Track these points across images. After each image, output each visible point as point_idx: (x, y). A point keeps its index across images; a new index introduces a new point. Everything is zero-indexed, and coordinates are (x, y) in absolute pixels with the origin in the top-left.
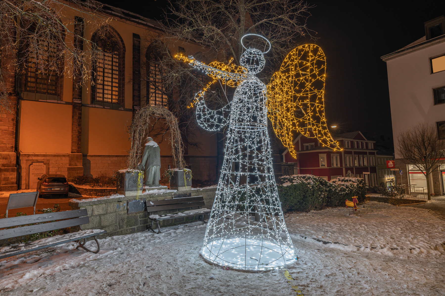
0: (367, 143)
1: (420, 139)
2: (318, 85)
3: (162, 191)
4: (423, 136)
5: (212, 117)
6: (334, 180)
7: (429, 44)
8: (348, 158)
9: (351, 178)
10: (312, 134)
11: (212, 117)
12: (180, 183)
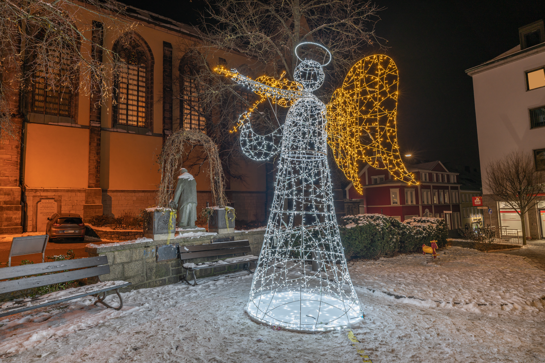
0: (448, 176)
1: (513, 171)
2: (389, 104)
3: (199, 234)
4: (517, 167)
5: (260, 144)
6: (409, 220)
7: (524, 54)
8: (425, 193)
9: (429, 219)
10: (381, 165)
11: (260, 144)
12: (220, 224)
